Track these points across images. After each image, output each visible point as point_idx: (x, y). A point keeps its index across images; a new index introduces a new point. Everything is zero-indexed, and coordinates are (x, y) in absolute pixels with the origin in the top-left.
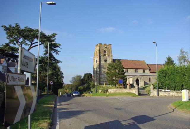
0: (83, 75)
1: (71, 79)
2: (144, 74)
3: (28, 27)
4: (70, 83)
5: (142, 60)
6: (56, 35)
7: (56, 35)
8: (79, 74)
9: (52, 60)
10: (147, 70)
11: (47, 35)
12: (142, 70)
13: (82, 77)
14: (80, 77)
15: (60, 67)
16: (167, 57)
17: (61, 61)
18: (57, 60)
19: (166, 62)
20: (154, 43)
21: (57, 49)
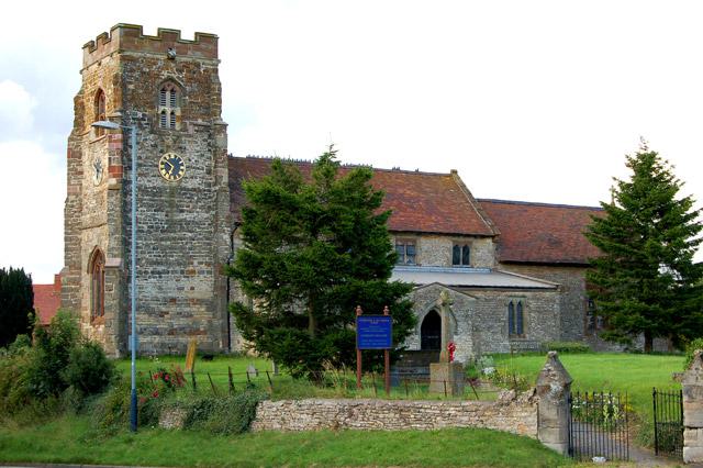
11: (477, 195)
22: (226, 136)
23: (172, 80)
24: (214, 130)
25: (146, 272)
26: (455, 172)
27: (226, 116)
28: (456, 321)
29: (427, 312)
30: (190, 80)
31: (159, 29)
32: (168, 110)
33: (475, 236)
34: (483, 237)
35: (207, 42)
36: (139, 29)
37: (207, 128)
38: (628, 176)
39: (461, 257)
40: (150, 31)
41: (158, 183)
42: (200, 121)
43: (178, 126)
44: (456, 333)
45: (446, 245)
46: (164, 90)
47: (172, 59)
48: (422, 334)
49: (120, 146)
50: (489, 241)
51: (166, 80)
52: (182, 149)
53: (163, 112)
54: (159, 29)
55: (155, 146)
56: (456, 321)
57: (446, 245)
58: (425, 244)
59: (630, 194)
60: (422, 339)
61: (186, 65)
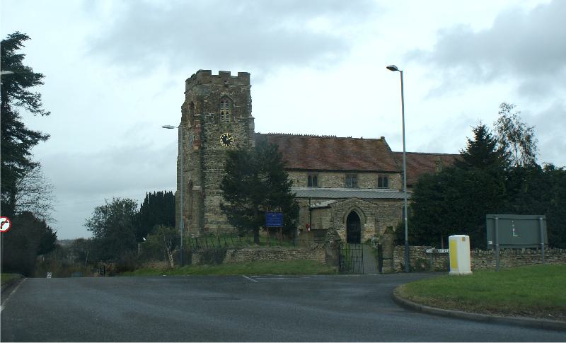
0: (139, 199)
1: (90, 215)
2: (383, 192)
3: (558, 165)
4: (88, 235)
5: (374, 135)
6: (24, 37)
7: (24, 37)
8: (123, 196)
9: (12, 133)
10: (394, 175)
11: (393, 150)
12: (373, 178)
13: (139, 208)
14: (129, 205)
15: (103, 210)
16: (476, 126)
17: (43, 135)
18: (31, 134)
19: (471, 142)
20: (393, 69)
21: (32, 90)
22: (254, 124)
23: (227, 96)
24: (249, 121)
25: (213, 193)
26: (383, 138)
27: (254, 114)
28: (365, 217)
29: (349, 212)
30: (235, 96)
31: (220, 71)
32: (225, 111)
33: (391, 172)
34: (395, 173)
35: (383, 138)
36: (210, 72)
37: (244, 120)
38: (473, 138)
39: (383, 183)
40: (215, 73)
41: (220, 148)
42: (241, 117)
43: (230, 119)
44: (366, 223)
45: (374, 177)
46: (222, 102)
47: (226, 86)
48: (347, 223)
49: (200, 130)
50: (398, 174)
51: (223, 97)
52: (232, 131)
53: (223, 113)
54: (220, 71)
55: (218, 130)
56: (365, 217)
57: (374, 177)
58: (361, 177)
59: (473, 147)
60: (347, 231)
61: (234, 89)
